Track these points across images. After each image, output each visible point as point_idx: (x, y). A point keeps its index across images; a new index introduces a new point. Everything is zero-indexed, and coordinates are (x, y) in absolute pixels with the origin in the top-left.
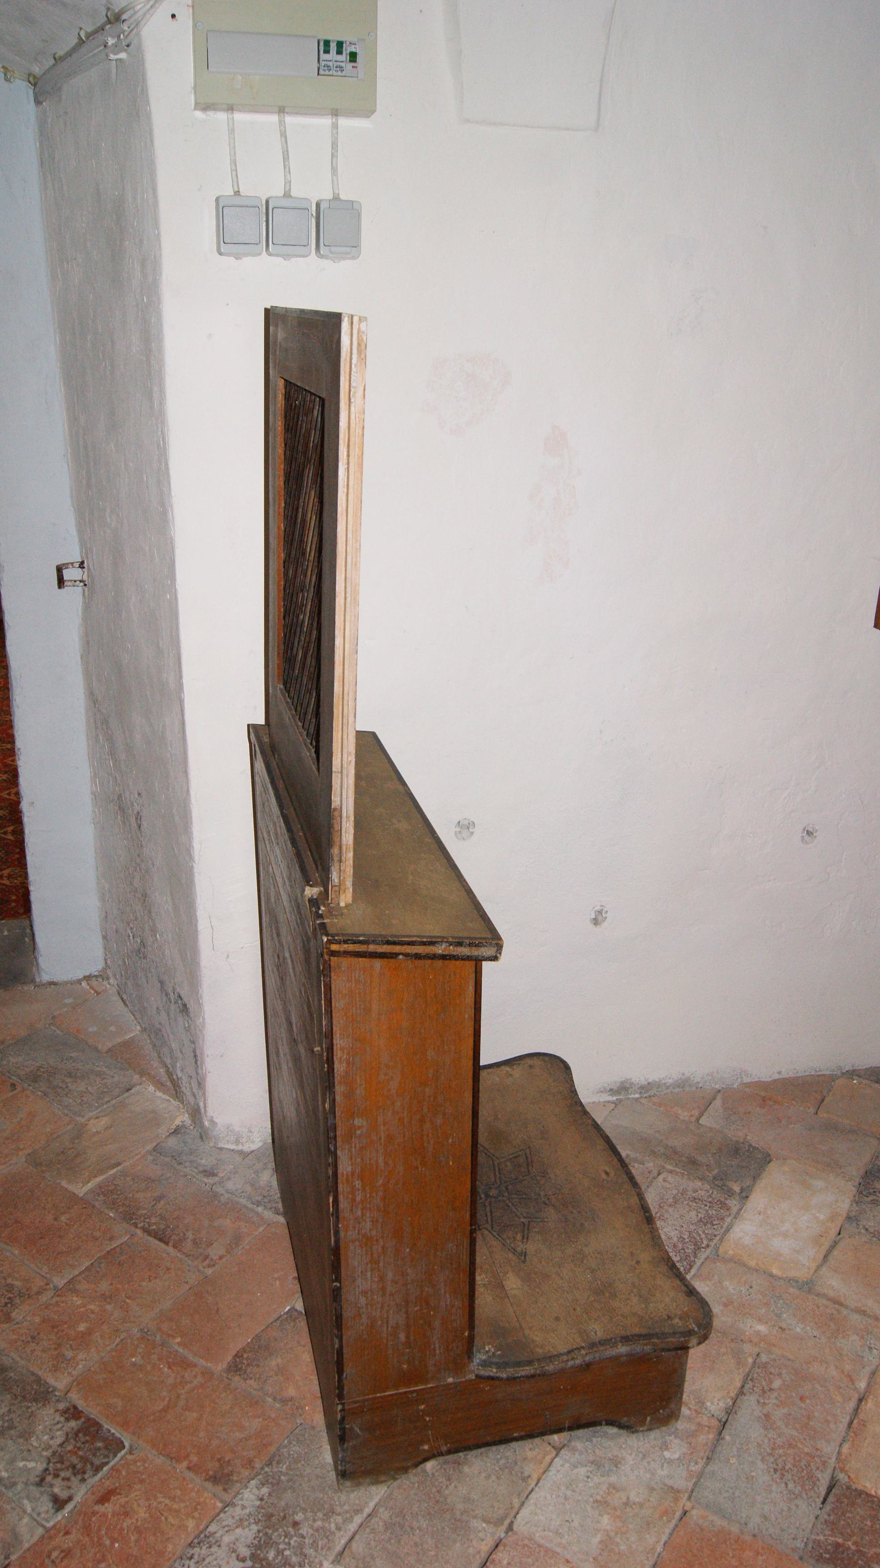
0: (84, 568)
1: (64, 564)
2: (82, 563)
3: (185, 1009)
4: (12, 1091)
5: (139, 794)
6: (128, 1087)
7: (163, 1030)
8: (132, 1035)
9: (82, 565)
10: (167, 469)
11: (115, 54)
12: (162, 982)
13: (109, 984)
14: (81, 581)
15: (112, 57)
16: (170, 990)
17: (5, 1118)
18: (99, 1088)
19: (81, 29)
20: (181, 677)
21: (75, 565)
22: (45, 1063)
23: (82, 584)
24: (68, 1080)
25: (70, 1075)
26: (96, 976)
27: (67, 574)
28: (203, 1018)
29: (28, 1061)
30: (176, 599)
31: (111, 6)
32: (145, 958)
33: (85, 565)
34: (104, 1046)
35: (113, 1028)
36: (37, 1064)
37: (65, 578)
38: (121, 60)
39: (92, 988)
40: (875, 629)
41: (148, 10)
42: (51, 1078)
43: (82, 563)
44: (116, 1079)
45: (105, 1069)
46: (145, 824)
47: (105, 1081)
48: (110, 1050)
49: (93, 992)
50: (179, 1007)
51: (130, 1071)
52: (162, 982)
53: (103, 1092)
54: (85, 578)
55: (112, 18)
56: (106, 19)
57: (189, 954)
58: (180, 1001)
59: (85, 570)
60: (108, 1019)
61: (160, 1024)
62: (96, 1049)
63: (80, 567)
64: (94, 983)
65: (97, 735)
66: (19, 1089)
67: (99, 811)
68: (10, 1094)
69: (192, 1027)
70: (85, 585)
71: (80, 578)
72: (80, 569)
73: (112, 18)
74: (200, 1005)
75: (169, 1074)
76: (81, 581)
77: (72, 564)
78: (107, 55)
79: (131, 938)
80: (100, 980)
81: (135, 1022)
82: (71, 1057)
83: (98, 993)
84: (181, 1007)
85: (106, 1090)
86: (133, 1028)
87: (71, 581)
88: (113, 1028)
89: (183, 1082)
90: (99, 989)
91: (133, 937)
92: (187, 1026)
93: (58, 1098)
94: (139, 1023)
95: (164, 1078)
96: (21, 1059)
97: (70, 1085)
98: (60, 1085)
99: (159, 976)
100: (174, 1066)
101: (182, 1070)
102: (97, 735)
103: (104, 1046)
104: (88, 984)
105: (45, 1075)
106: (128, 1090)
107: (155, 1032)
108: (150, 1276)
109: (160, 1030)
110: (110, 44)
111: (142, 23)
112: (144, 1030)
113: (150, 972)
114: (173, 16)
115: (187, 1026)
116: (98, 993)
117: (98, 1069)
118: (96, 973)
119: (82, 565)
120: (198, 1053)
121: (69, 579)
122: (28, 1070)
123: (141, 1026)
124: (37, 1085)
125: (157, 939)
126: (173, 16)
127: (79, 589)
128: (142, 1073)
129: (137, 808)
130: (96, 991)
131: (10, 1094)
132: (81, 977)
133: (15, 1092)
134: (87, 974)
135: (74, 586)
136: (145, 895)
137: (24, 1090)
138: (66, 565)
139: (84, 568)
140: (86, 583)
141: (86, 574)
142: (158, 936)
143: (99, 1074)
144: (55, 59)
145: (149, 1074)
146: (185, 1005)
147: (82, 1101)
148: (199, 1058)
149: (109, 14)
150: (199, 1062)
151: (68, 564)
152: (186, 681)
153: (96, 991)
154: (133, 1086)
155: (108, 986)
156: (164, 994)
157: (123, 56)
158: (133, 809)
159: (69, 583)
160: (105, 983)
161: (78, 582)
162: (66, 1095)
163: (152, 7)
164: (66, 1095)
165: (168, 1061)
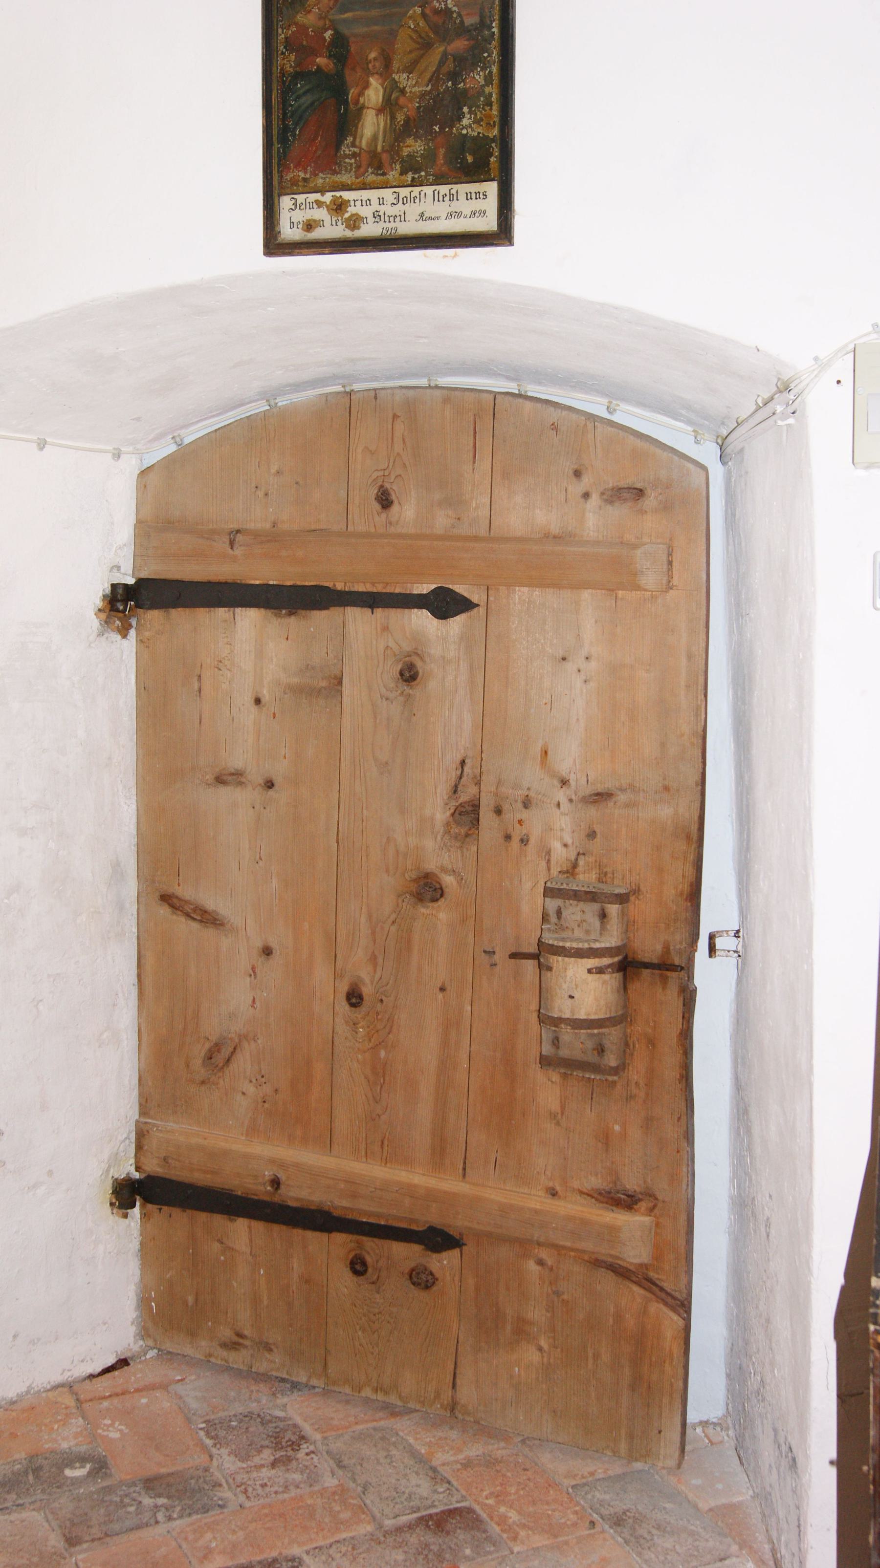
0: (739, 937)
1: (718, 932)
2: (738, 931)
3: (793, 1464)
4: (590, 1529)
5: (770, 1196)
6: (722, 1555)
7: (773, 1495)
8: (741, 1499)
9: (737, 934)
10: (811, 829)
11: (782, 420)
12: (775, 1431)
13: (728, 1435)
14: (735, 952)
15: (780, 423)
16: (782, 1441)
17: (575, 1556)
18: (689, 1549)
19: (758, 396)
20: (812, 1057)
21: (729, 933)
22: (633, 1507)
23: (736, 955)
24: (654, 1531)
25: (658, 1527)
26: (714, 1424)
27: (719, 943)
28: (810, 1475)
29: (616, 1500)
30: (812, 969)
31: (780, 377)
32: (763, 1400)
33: (741, 934)
34: (703, 1506)
35: (720, 1486)
36: (624, 1507)
37: (717, 947)
38: (789, 425)
39: (707, 1436)
40: (711, 959)
41: (812, 380)
42: (637, 1526)
43: (738, 931)
44: (711, 1544)
45: (701, 1530)
46: (773, 1232)
47: (697, 1543)
48: (711, 1510)
49: (707, 1441)
50: (789, 1462)
51: (729, 1539)
52: (775, 1431)
53: (691, 1555)
54: (740, 948)
55: (781, 387)
56: (776, 389)
57: (801, 1392)
58: (790, 1454)
59: (741, 939)
60: (717, 1474)
61: (771, 1486)
62: (696, 1507)
63: (735, 936)
64: (710, 1430)
65: (739, 1128)
66: (598, 1528)
67: (735, 1218)
68: (587, 1532)
69: (799, 1488)
70: (739, 956)
71: (735, 949)
72: (735, 938)
73: (781, 387)
74: (807, 1457)
75: (774, 1551)
76: (735, 952)
77: (727, 932)
78: (776, 422)
79: (753, 1375)
80: (718, 1429)
81: (748, 1485)
82: (665, 1508)
83: (712, 1443)
84: (791, 1461)
85: (696, 1553)
86: (744, 1491)
87: (724, 950)
88: (720, 1486)
89: (786, 1561)
90: (714, 1440)
91: (754, 1374)
92: (794, 1485)
93: (640, 1549)
94: (752, 1487)
95: (768, 1556)
96: (607, 1497)
97: (655, 1538)
98: (646, 1535)
99: (773, 1424)
100: (779, 1540)
101: (787, 1545)
102: (739, 1128)
103: (703, 1506)
104: (704, 1432)
105: (631, 1521)
106: (721, 1560)
107: (763, 1497)
108: (391, 1303)
109: (770, 1494)
110: (778, 411)
111: (806, 392)
112: (755, 1496)
113: (767, 1418)
114: (839, 382)
115: (794, 1485)
116: (712, 1443)
117: (693, 1528)
118: (715, 1420)
119: (737, 934)
120: (802, 1522)
121: (721, 948)
122: (612, 1510)
123: (754, 1492)
124: (619, 1529)
125: (775, 1375)
126: (839, 382)
127: (733, 960)
128: (743, 1545)
129: (767, 1212)
130: (710, 1441)
131: (587, 1532)
132: (697, 1421)
133: (592, 1531)
134: (705, 1418)
135: (727, 956)
136: (768, 1321)
137: (603, 1531)
138: (720, 933)
139: (739, 937)
140: (740, 954)
141: (741, 944)
142: (776, 1372)
143: (692, 1534)
144: (737, 423)
145: (751, 1547)
146: (794, 1460)
147: (666, 1559)
148: (802, 1528)
149: (779, 384)
150: (802, 1534)
151: (723, 931)
152: (816, 1062)
153: (710, 1441)
154: (729, 1557)
155: (726, 1438)
156: (777, 1446)
157: (791, 421)
158: (763, 1214)
159: (722, 953)
160: (724, 1433)
161: (732, 952)
162: (649, 1548)
163: (816, 376)
164: (649, 1548)
165: (774, 1534)
